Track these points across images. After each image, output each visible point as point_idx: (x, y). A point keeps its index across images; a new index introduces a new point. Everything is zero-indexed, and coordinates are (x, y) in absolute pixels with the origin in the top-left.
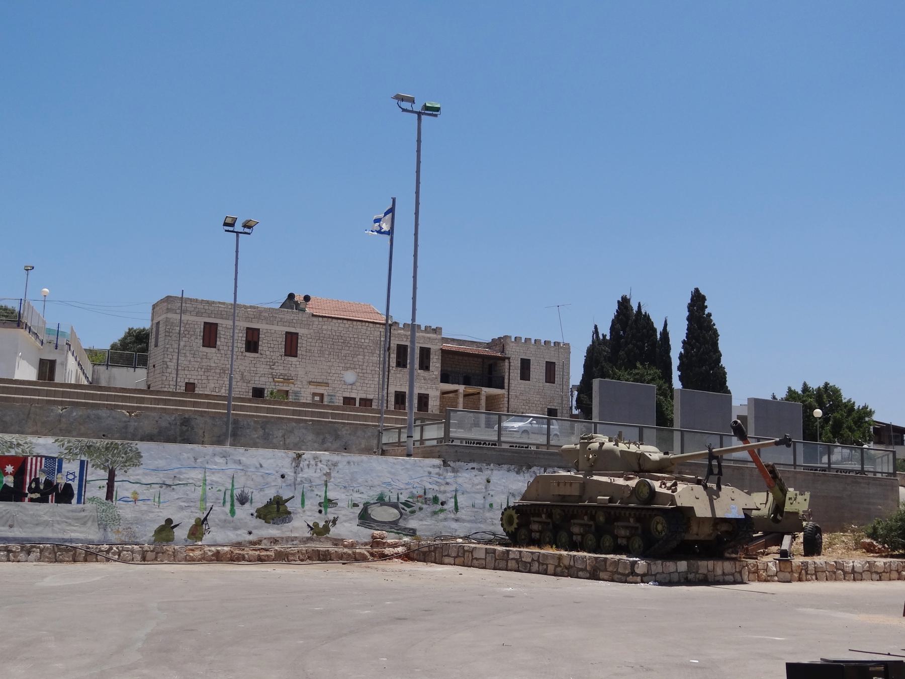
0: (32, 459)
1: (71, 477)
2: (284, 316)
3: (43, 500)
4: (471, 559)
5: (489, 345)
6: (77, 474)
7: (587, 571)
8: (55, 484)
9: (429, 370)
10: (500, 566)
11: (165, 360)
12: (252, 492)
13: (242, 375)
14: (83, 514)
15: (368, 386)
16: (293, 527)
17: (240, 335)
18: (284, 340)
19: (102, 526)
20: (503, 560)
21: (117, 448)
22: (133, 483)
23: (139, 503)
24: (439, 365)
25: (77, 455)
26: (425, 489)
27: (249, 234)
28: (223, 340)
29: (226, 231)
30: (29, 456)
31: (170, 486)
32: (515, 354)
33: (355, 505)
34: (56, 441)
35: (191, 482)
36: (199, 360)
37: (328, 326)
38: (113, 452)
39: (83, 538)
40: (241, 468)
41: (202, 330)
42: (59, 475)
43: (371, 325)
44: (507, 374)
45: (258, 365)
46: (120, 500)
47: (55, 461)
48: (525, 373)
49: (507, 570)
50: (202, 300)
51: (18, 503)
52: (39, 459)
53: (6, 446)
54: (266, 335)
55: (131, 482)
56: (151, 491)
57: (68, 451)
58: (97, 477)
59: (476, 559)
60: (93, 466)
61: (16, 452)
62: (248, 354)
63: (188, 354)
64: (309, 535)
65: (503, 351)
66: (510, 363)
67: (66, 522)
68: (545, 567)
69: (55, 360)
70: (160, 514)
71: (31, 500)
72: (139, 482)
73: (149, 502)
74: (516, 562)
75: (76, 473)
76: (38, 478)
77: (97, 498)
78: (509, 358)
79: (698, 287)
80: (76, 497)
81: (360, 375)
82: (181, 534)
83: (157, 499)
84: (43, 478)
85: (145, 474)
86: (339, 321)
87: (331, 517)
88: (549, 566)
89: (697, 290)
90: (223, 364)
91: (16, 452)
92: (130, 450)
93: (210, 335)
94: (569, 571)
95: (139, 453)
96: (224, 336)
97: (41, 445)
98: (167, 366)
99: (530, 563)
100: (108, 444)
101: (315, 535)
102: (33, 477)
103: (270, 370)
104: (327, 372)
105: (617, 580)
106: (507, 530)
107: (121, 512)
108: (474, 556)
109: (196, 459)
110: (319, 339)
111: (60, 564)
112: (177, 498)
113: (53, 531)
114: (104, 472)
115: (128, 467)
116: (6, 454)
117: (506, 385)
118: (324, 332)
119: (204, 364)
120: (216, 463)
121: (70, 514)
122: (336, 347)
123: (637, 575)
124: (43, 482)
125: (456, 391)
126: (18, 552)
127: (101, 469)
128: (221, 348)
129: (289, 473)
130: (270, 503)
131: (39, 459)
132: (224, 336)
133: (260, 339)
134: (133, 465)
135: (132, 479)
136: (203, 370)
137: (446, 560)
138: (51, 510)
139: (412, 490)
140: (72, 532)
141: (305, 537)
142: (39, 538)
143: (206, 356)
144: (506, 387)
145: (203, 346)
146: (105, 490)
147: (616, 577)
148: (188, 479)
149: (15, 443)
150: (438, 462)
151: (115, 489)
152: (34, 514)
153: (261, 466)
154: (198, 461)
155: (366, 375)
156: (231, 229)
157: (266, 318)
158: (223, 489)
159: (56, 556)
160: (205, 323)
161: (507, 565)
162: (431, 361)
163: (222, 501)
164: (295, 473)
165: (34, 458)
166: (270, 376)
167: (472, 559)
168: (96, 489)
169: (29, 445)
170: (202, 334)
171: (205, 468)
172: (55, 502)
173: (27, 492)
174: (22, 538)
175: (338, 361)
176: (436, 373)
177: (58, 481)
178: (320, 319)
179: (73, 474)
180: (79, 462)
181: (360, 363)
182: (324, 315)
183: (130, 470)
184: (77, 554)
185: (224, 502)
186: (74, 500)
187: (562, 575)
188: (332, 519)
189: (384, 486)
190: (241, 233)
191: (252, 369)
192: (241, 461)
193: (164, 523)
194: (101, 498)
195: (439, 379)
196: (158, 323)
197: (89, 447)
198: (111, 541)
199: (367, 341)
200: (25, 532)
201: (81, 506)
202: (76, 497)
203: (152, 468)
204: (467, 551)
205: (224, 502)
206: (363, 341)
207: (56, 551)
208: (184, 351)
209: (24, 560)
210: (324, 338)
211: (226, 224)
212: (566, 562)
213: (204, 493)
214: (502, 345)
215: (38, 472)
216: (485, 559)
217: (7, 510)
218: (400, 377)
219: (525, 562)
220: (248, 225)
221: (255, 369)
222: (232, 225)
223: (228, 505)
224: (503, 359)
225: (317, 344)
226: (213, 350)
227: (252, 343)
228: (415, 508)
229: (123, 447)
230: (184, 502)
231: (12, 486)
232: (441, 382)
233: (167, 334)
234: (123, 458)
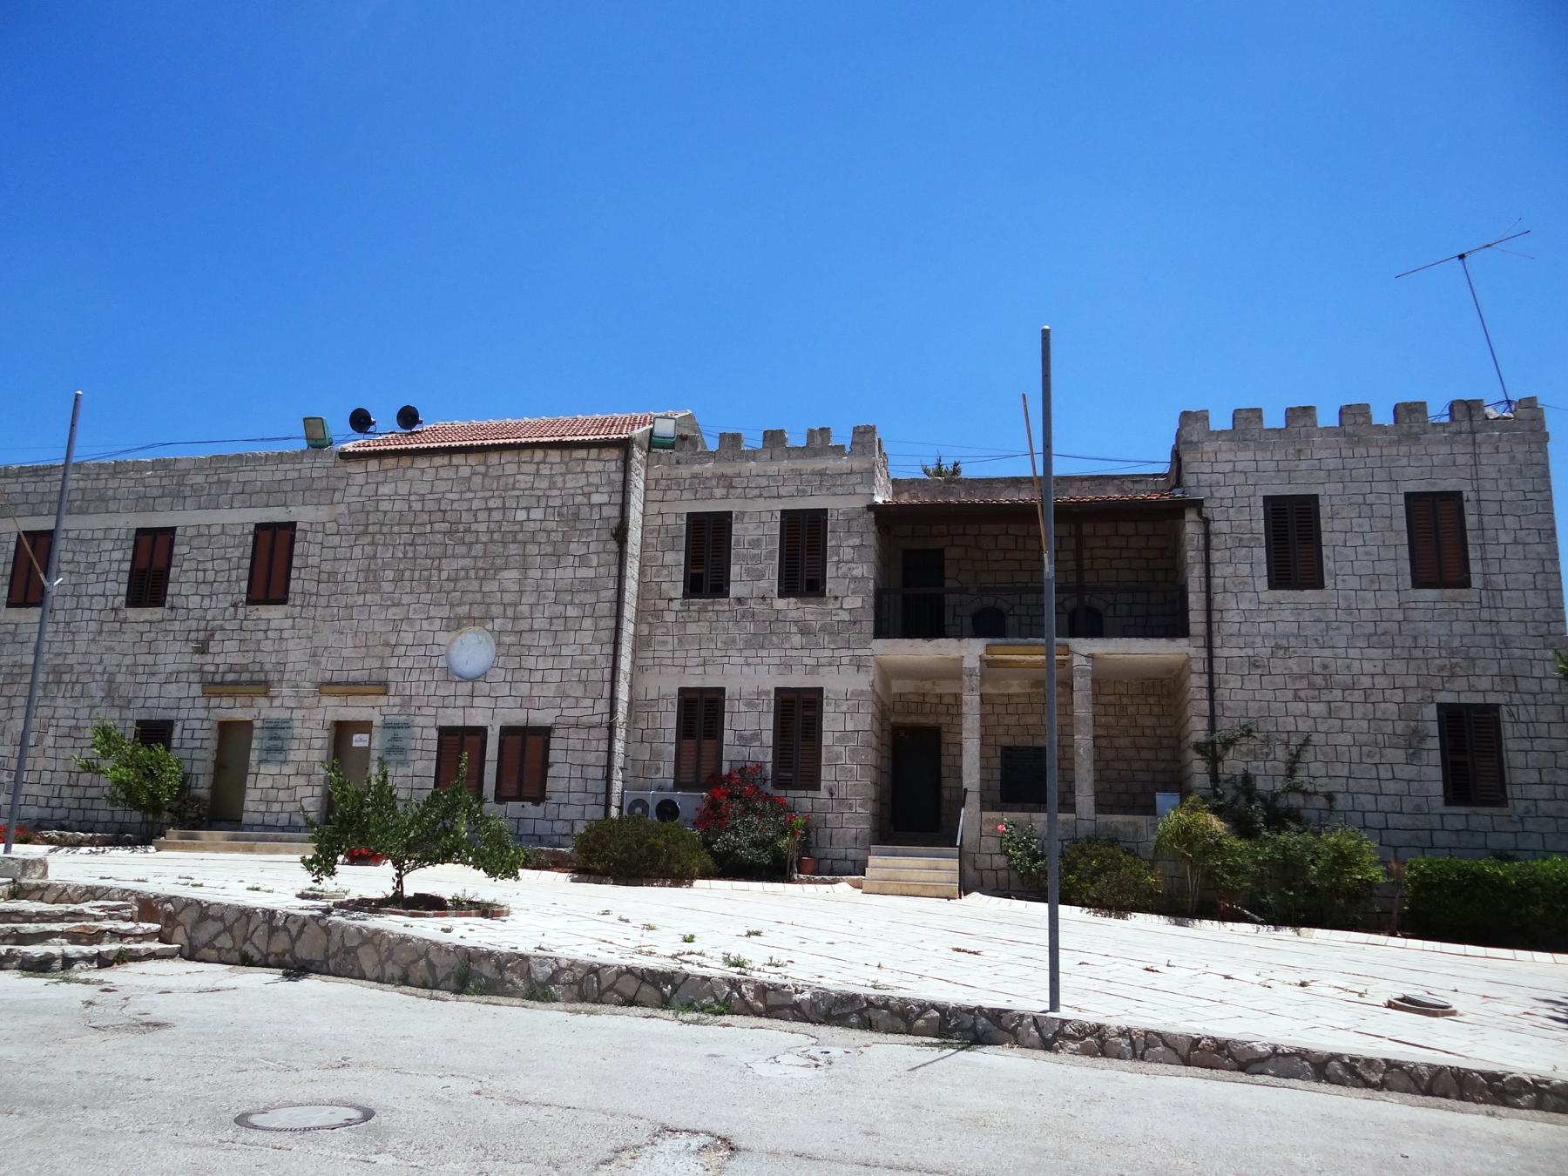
15: (538, 677)
18: (249, 551)
24: (864, 570)
43: (554, 456)
66: (1206, 522)
78: (1198, 505)
104: (387, 644)
117: (1196, 617)
118: (385, 506)
162: (831, 559)
166: (194, 677)
175: (427, 598)
176: (853, 602)
181: (508, 598)
195: (868, 626)
206: (521, 515)
210: (382, 524)
221: (150, 659)
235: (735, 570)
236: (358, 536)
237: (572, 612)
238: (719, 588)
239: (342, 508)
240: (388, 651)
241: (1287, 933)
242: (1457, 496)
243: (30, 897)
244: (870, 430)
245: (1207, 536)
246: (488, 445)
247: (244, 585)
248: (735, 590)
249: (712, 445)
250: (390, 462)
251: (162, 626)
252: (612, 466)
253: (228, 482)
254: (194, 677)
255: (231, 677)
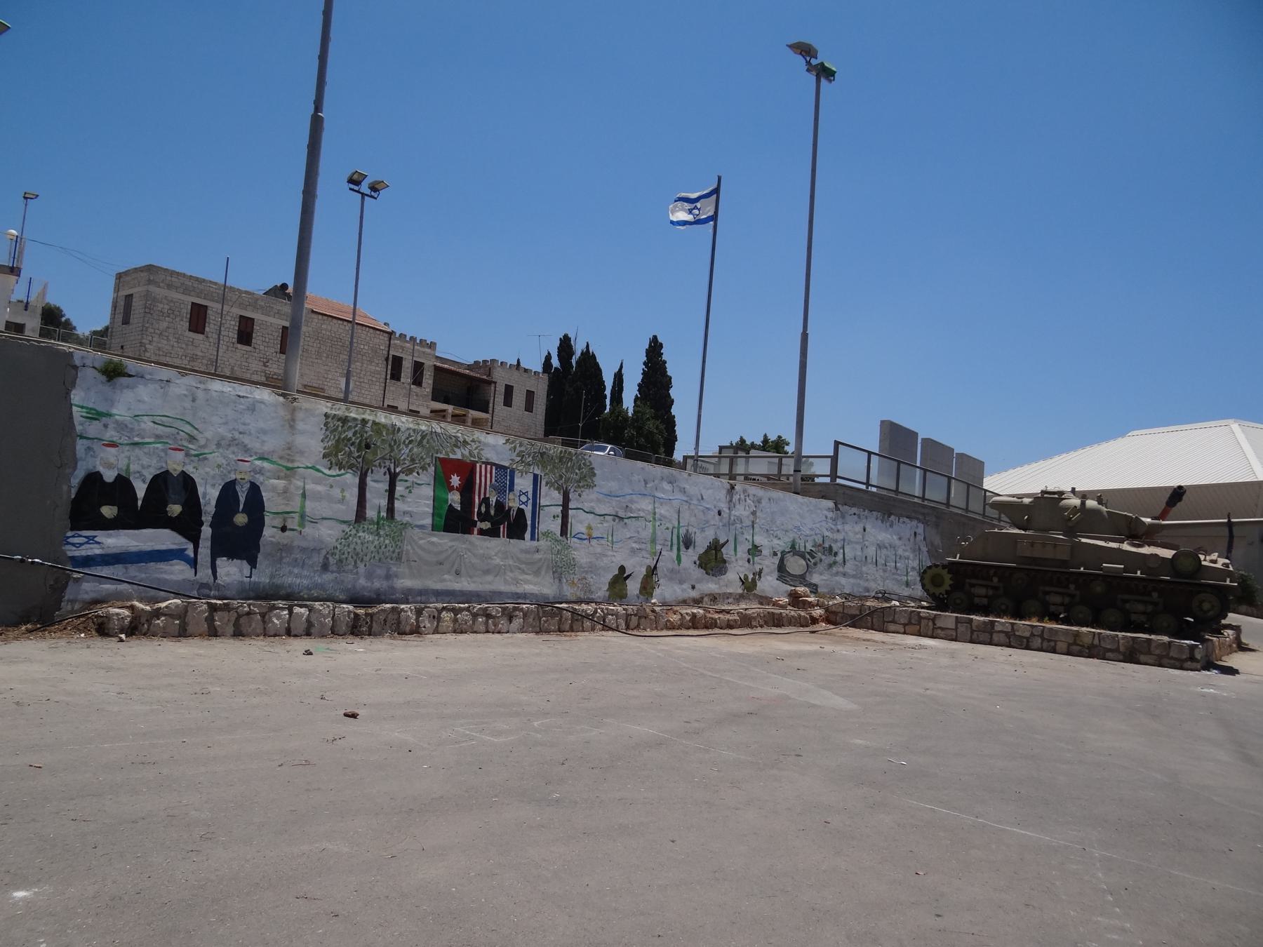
0: (481, 467)
1: (524, 499)
2: (281, 308)
3: (493, 533)
4: (931, 628)
5: (469, 367)
6: (530, 496)
7: (1119, 652)
8: (507, 508)
9: (421, 386)
10: (981, 639)
11: (144, 341)
12: (695, 533)
13: (232, 369)
14: (537, 556)
15: (365, 396)
16: (728, 581)
17: (233, 323)
18: (280, 335)
19: (556, 575)
20: (984, 632)
21: (571, 460)
22: (587, 512)
23: (594, 542)
24: (431, 382)
25: (530, 465)
26: (379, 507)
27: (376, 198)
28: (212, 326)
29: (351, 189)
30: (477, 462)
31: (622, 519)
32: (501, 378)
33: (775, 554)
34: (507, 441)
35: (641, 515)
36: (184, 346)
37: (327, 326)
38: (567, 465)
39: (537, 592)
40: (685, 499)
41: (189, 311)
42: (511, 496)
43: (371, 331)
44: (492, 398)
45: (250, 360)
46: (574, 537)
47: (507, 473)
48: (508, 402)
49: (991, 643)
50: (191, 276)
51: (466, 536)
52: (489, 467)
53: (450, 444)
54: (262, 326)
55: (585, 511)
56: (605, 525)
57: (519, 458)
58: (551, 497)
59: (940, 628)
60: (547, 483)
61: (462, 454)
62: (239, 346)
63: (171, 338)
64: (740, 591)
65: (489, 375)
66: (495, 387)
67: (520, 569)
68: (1052, 644)
69: (24, 324)
70: (613, 559)
71: (481, 532)
72: (592, 510)
73: (603, 542)
74: (1006, 636)
75: (529, 493)
76: (489, 498)
77: (551, 532)
78: (495, 383)
79: (656, 334)
80: (529, 529)
81: (357, 383)
82: (633, 587)
83: (610, 539)
84: (493, 500)
85: (598, 500)
86: (340, 322)
87: (757, 568)
88: (1058, 643)
89: (655, 337)
90: (211, 355)
91: (462, 454)
92: (584, 464)
93: (198, 317)
94: (1131, 655)
95: (593, 468)
96: (214, 322)
97: (490, 446)
98: (146, 348)
99: (1028, 639)
100: (561, 451)
101: (745, 591)
102: (482, 496)
103: (263, 368)
104: (324, 377)
105: (1168, 666)
106: (931, 592)
107: (575, 554)
108: (938, 625)
109: (646, 483)
110: (318, 339)
111: (559, 638)
112: (628, 536)
113: (506, 582)
114: (558, 495)
115: (583, 489)
116: (452, 456)
117: (491, 409)
118: (324, 332)
119: (189, 351)
120: (664, 491)
121: (523, 556)
122: (334, 350)
123: (1197, 661)
124: (494, 505)
125: (444, 411)
126: (498, 617)
127: (555, 489)
128: (210, 335)
129: (724, 506)
130: (709, 548)
131: (489, 467)
132: (214, 322)
133: (255, 331)
134: (587, 485)
135: (587, 506)
136: (188, 358)
137: (892, 627)
138: (503, 549)
139: (815, 537)
140: (526, 583)
141: (737, 594)
142: (490, 592)
143: (192, 342)
144: (490, 412)
145: (190, 330)
146: (559, 521)
147: (1165, 661)
148: (639, 510)
149: (461, 440)
150: (830, 504)
151: (570, 520)
152: (484, 554)
153: (702, 498)
154: (648, 486)
155: (363, 384)
156: (356, 188)
157: (262, 307)
158: (670, 526)
159: (540, 622)
160: (193, 303)
161: (991, 638)
162: (424, 378)
163: (669, 544)
164: (729, 509)
165: (483, 466)
166: (263, 374)
167: (934, 628)
168: (549, 522)
169: (478, 444)
170: (189, 316)
171: (654, 496)
172: (508, 537)
173: (476, 519)
174: (470, 591)
175: (336, 365)
176: (428, 390)
177: (510, 505)
178: (320, 317)
179: (526, 494)
180: (532, 475)
181: (358, 371)
182: (324, 312)
183: (584, 493)
184: (563, 619)
185: (672, 545)
186: (528, 535)
187: (1079, 654)
188: (758, 570)
189: (795, 530)
190: (367, 195)
191: (244, 364)
192: (686, 490)
193: (617, 572)
194: (556, 533)
195: (430, 397)
196: (129, 298)
197: (542, 454)
198: (565, 598)
199: (366, 347)
200: (474, 582)
201: (535, 543)
202: (529, 529)
203: (605, 493)
204: (925, 618)
205: (672, 545)
206: (362, 347)
207: (541, 615)
208: (167, 334)
209: (505, 631)
210: (323, 338)
211: (351, 181)
212: (1088, 640)
213: (654, 532)
214: (488, 369)
215: (488, 488)
216: (956, 629)
217: (453, 546)
218: (393, 391)
219: (1019, 636)
220: (374, 188)
221: (247, 364)
222: (357, 183)
223: (675, 548)
224: (489, 383)
225: (315, 344)
226: (201, 337)
227: (245, 333)
228: (817, 559)
229: (576, 458)
230: (635, 542)
231: (459, 509)
232: (433, 400)
233: (147, 310)
234: (577, 474)
235: (402, 374)
236: (315, 340)
237: (374, 379)
238: (398, 379)
239: (310, 329)
240: (324, 379)
241: (1112, 442)
242: (534, 392)
243: (1170, 492)
244: (435, 344)
245: (495, 390)
246: (1087, 627)
247: (279, 346)
248: (402, 380)
249: (408, 339)
250: (325, 318)
251: (250, 353)
252: (386, 339)
253: (273, 308)
254: (263, 374)
255: (275, 377)
